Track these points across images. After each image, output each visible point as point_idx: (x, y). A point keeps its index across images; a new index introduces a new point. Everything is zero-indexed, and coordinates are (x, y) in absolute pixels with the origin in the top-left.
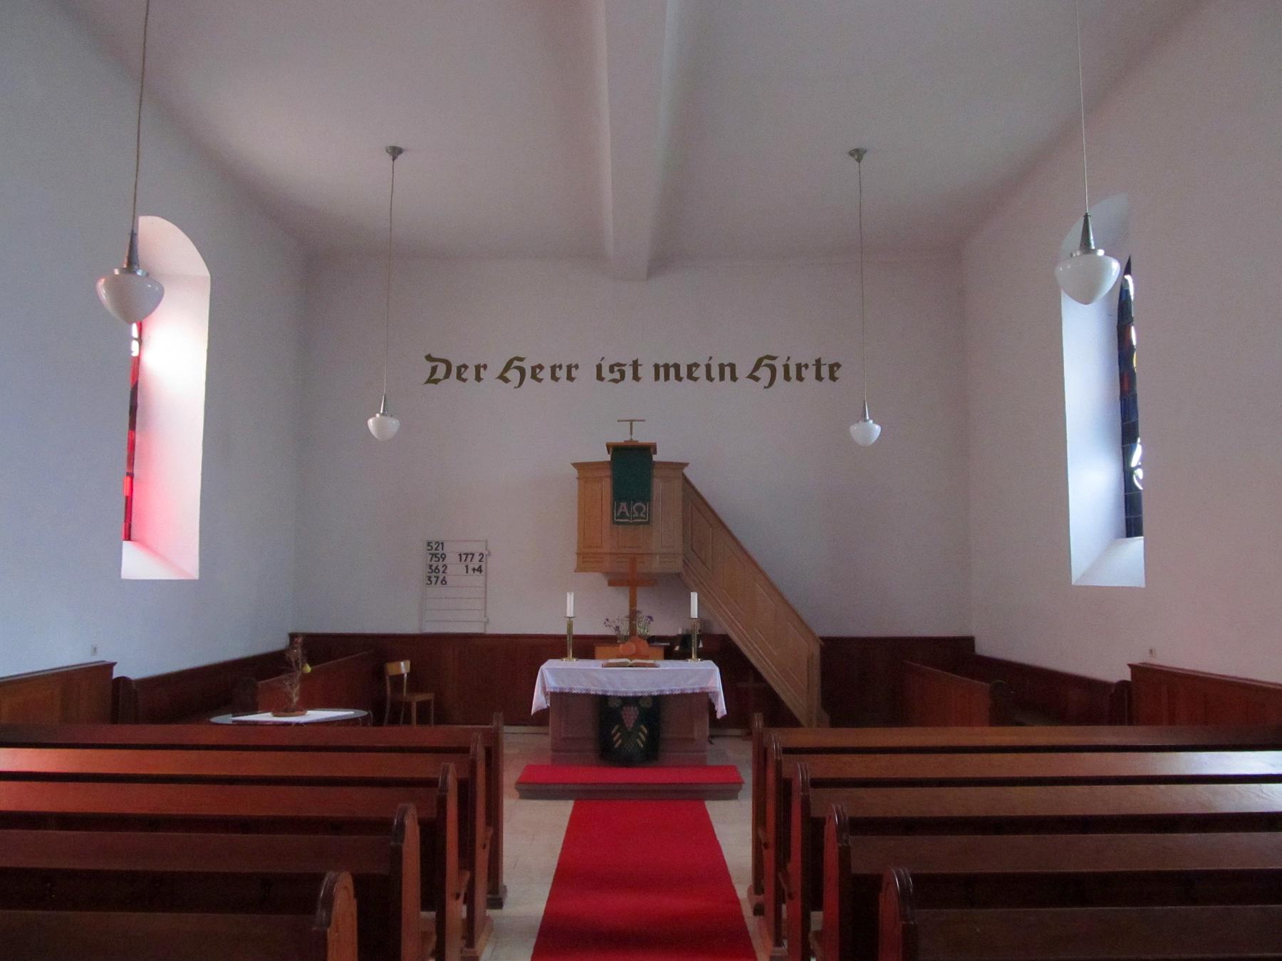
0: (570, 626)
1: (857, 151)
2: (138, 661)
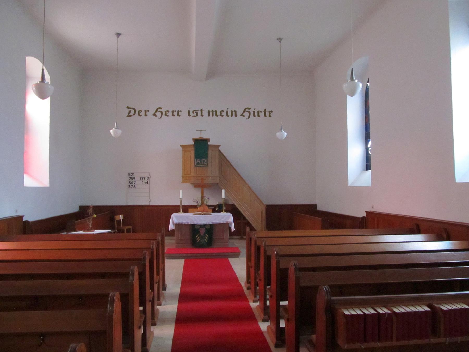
0: (181, 202)
1: (280, 38)
2: (32, 215)
